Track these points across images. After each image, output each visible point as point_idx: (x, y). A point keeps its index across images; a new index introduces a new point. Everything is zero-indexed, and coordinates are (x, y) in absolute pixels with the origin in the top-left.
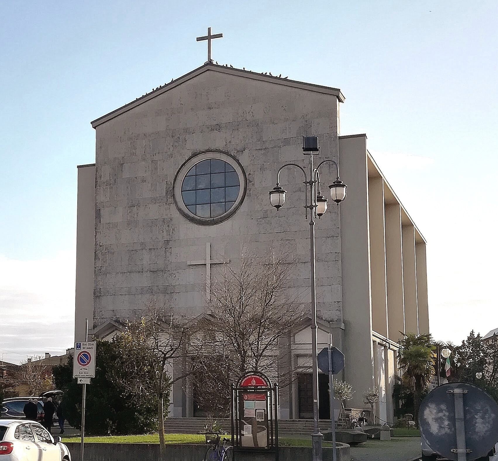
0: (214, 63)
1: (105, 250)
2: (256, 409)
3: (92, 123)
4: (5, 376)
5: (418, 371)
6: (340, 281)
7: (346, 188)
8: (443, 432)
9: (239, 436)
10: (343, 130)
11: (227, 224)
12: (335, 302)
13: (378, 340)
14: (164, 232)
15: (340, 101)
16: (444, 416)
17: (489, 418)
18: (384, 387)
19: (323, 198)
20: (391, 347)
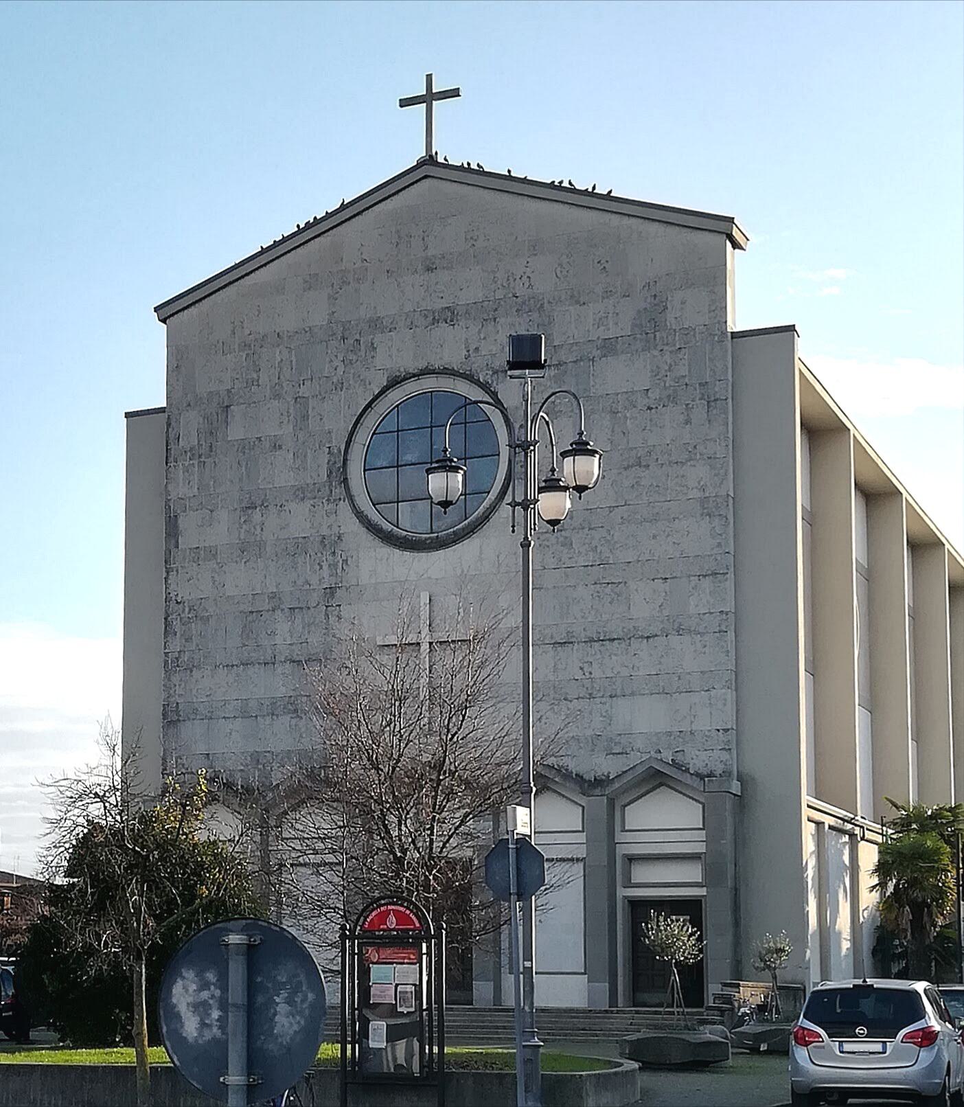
0: (441, 160)
1: (189, 613)
2: (397, 985)
3: (156, 309)
4: (7, 909)
5: (916, 894)
6: (730, 680)
7: (600, 459)
8: (208, 1035)
9: (427, 1051)
10: (741, 317)
11: (467, 550)
12: (718, 730)
13: (829, 821)
14: (324, 567)
15: (736, 245)
16: (213, 997)
17: (303, 1001)
18: (849, 931)
19: (561, 483)
20: (866, 837)
